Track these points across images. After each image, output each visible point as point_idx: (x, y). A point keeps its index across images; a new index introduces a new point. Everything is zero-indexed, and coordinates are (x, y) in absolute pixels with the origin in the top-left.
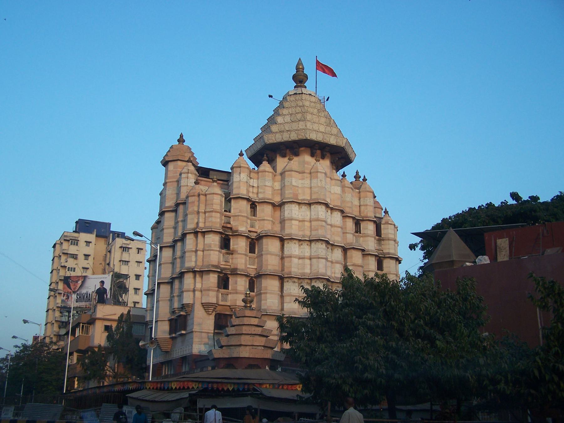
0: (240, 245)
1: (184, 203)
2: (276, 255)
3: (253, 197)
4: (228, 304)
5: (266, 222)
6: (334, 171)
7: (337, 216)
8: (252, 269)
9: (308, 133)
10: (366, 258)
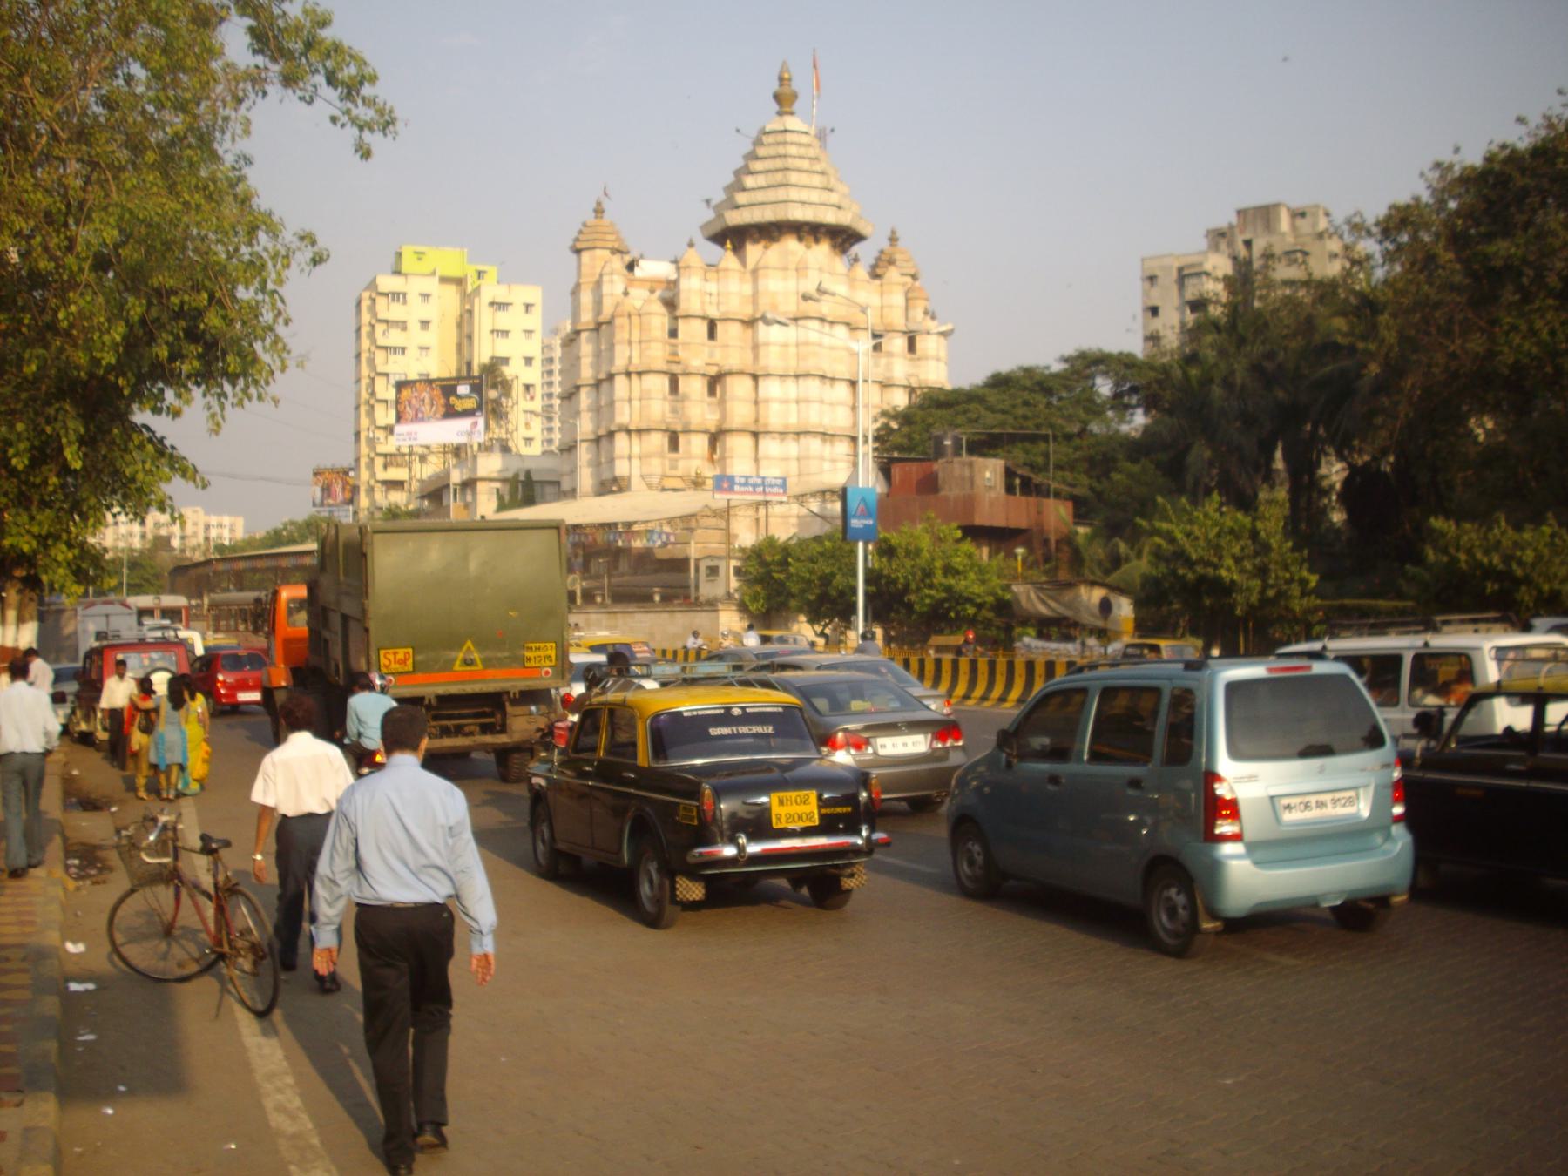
0: (694, 387)
1: (610, 323)
3: (713, 313)
7: (841, 331)
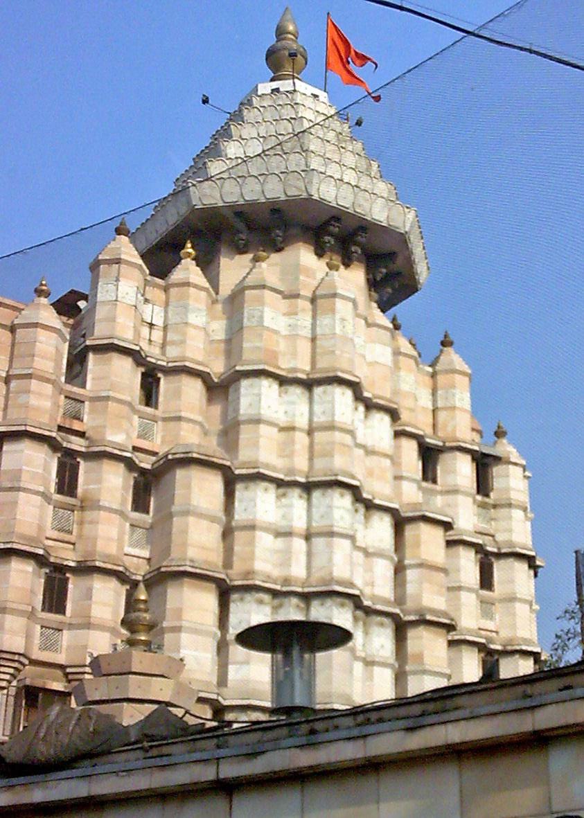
2: (213, 519)
3: (153, 354)
4: (61, 659)
5: (184, 425)
8: (138, 557)
9: (315, 180)
10: (453, 550)
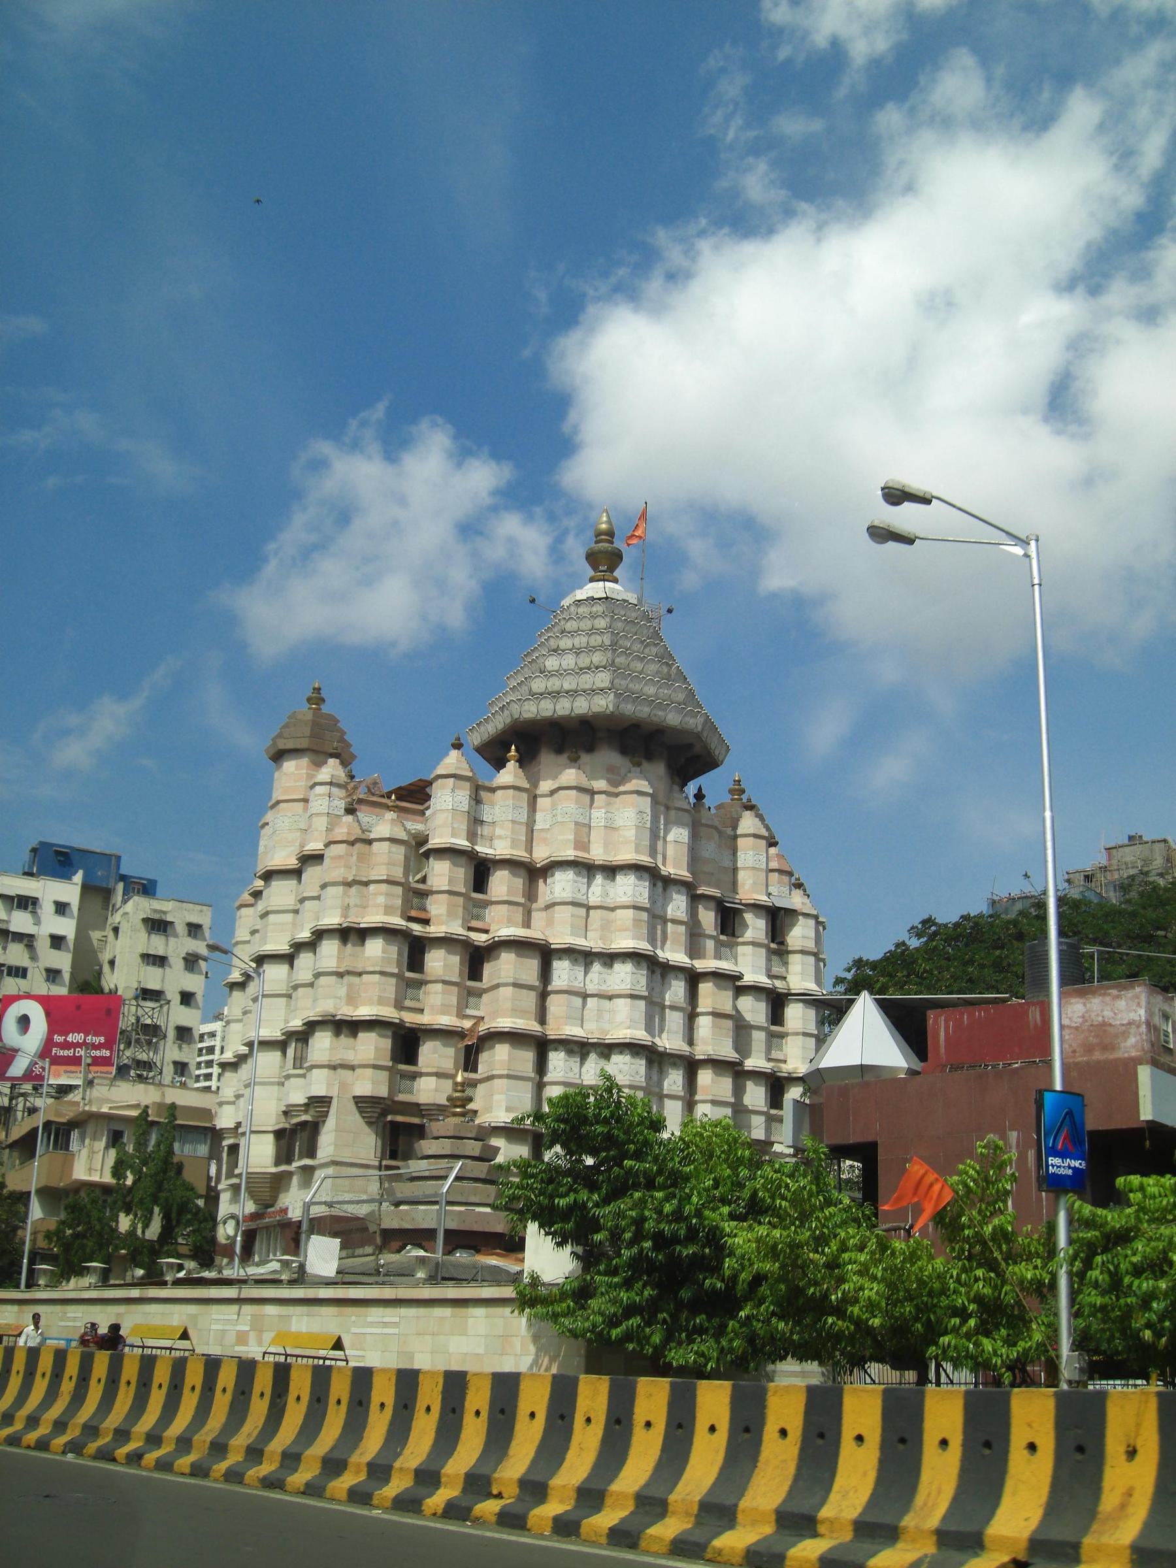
6: (676, 788)
